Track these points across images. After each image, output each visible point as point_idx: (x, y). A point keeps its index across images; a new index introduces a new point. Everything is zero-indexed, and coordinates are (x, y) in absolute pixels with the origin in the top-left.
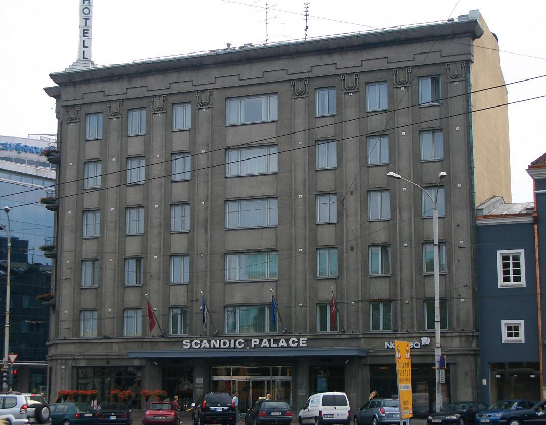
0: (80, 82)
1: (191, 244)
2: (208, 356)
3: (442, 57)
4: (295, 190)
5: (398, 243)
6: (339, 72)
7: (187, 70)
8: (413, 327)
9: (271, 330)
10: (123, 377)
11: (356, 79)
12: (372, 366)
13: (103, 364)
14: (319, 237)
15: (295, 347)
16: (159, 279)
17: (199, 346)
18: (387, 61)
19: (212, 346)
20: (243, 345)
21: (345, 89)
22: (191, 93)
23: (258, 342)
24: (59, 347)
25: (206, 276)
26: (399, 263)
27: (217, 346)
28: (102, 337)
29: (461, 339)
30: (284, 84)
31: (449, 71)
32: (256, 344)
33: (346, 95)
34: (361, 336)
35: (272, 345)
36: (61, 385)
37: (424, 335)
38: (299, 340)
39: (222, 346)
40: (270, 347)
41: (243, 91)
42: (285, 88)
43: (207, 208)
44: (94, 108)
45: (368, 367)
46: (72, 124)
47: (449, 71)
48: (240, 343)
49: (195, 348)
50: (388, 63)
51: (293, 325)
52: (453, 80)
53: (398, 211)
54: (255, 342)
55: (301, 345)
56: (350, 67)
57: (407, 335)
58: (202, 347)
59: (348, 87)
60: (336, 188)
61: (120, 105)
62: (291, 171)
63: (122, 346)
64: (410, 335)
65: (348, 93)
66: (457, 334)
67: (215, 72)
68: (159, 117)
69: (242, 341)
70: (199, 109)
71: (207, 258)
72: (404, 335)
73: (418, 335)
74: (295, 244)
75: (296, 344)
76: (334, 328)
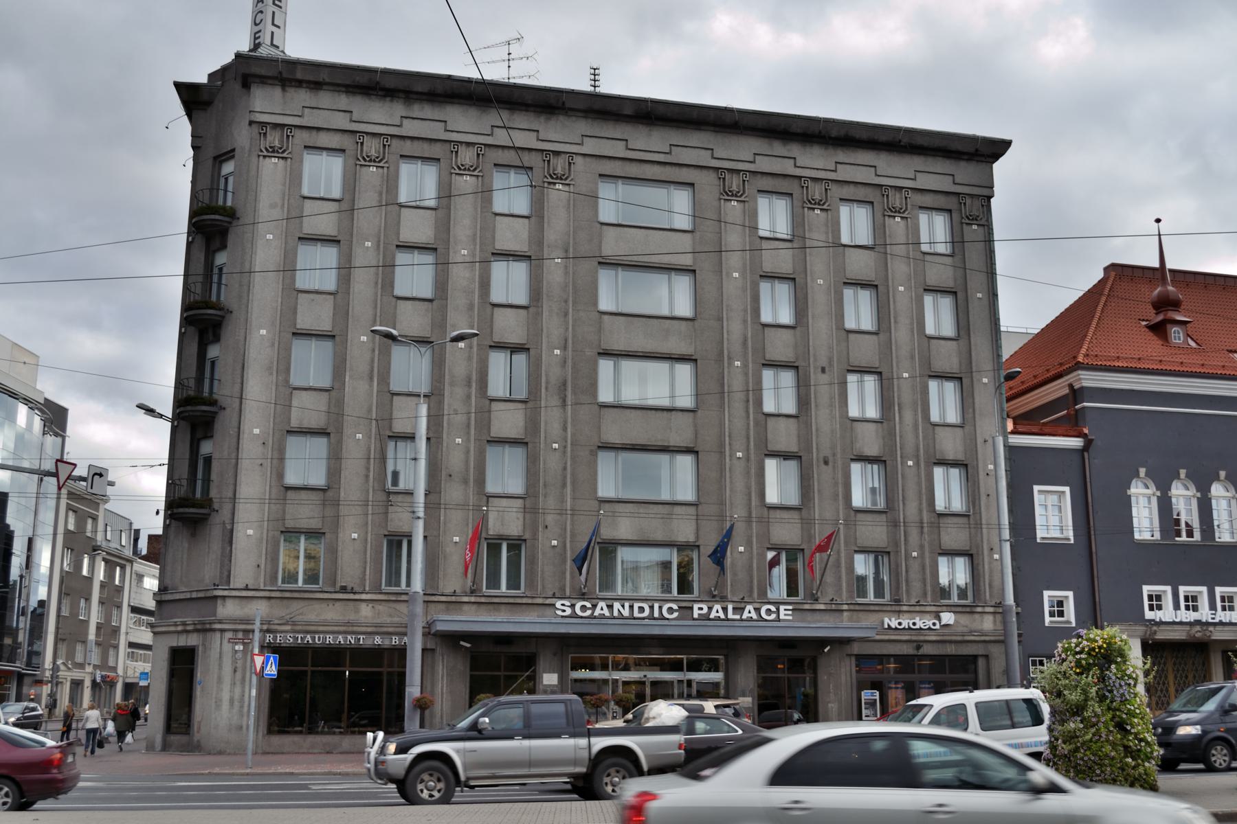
0: (299, 83)
1: (533, 424)
2: (531, 631)
3: (352, 121)
4: (729, 353)
5: (899, 459)
6: (798, 172)
7: (527, 111)
8: (925, 594)
9: (680, 592)
10: (309, 669)
11: (478, 155)
12: (860, 658)
13: (907, 650)
14: (770, 436)
15: (672, 619)
16: (465, 481)
17: (588, 613)
18: (797, 161)
19: (616, 614)
20: (676, 614)
21: (726, 193)
22: (534, 153)
23: (705, 610)
24: (229, 603)
25: (564, 485)
26: (900, 492)
27: (626, 613)
28: (338, 589)
29: (995, 617)
30: (705, 172)
31: (965, 208)
32: (701, 612)
33: (811, 212)
34: (845, 607)
35: (730, 616)
36: (233, 684)
37: (944, 608)
38: (778, 609)
39: (636, 614)
40: (728, 620)
41: (634, 170)
42: (706, 181)
43: (565, 362)
44: (324, 139)
45: (853, 659)
46: (275, 160)
47: (965, 208)
48: (670, 610)
49: (582, 617)
50: (446, 130)
51: (729, 583)
52: (461, 172)
53: (896, 408)
54: (701, 609)
55: (782, 617)
56: (817, 169)
57: (918, 608)
58: (596, 614)
59: (368, 157)
60: (797, 359)
61: (260, 133)
62: (720, 319)
63: (380, 607)
64: (922, 609)
65: (894, 217)
66: (991, 610)
67: (582, 126)
68: (466, 182)
69: (675, 607)
70: (550, 183)
71: (565, 452)
72: (912, 609)
73: (933, 609)
74: (730, 444)
75: (773, 616)
76: (514, 583)
